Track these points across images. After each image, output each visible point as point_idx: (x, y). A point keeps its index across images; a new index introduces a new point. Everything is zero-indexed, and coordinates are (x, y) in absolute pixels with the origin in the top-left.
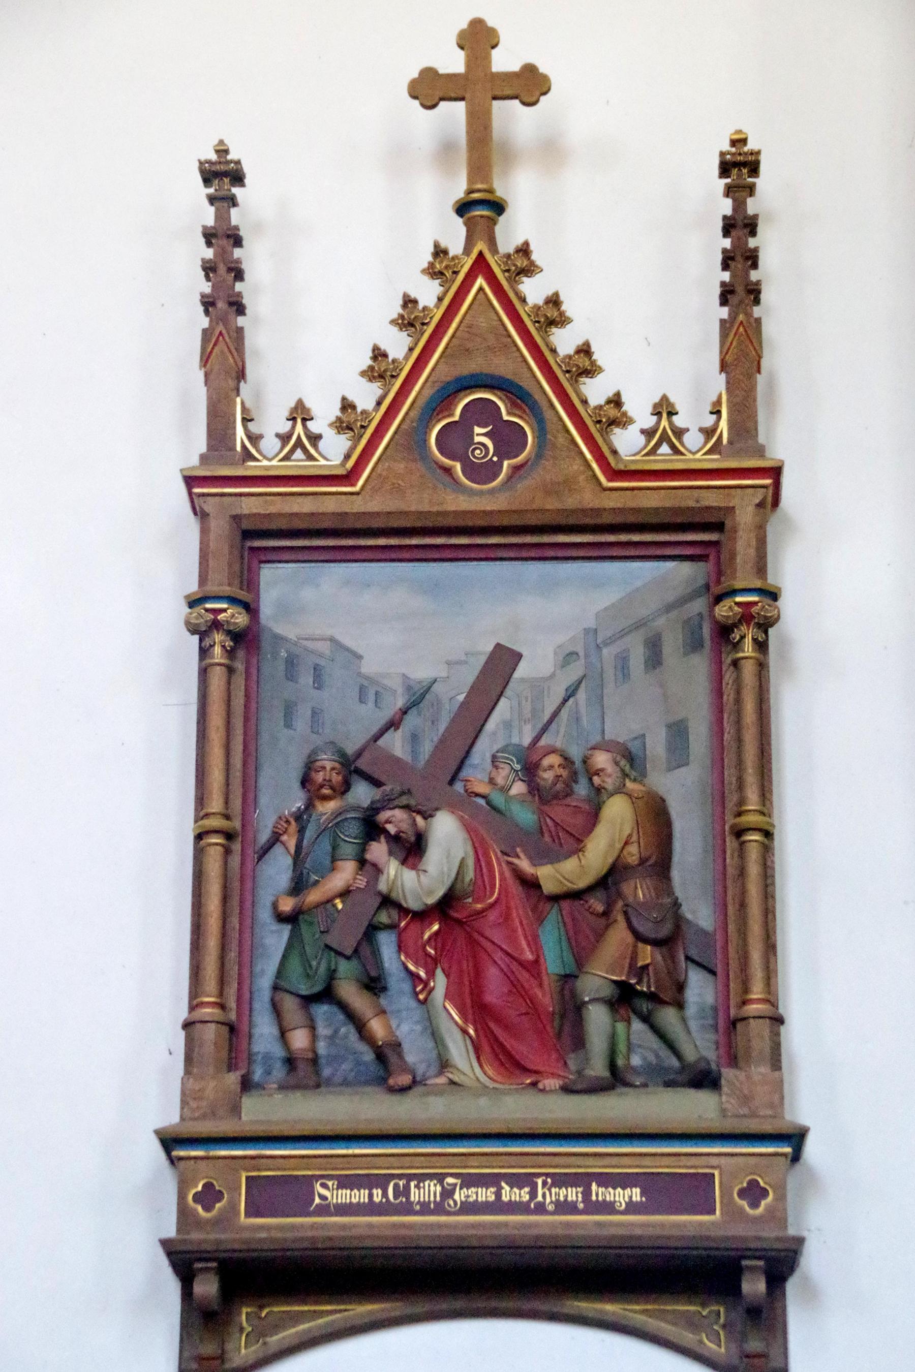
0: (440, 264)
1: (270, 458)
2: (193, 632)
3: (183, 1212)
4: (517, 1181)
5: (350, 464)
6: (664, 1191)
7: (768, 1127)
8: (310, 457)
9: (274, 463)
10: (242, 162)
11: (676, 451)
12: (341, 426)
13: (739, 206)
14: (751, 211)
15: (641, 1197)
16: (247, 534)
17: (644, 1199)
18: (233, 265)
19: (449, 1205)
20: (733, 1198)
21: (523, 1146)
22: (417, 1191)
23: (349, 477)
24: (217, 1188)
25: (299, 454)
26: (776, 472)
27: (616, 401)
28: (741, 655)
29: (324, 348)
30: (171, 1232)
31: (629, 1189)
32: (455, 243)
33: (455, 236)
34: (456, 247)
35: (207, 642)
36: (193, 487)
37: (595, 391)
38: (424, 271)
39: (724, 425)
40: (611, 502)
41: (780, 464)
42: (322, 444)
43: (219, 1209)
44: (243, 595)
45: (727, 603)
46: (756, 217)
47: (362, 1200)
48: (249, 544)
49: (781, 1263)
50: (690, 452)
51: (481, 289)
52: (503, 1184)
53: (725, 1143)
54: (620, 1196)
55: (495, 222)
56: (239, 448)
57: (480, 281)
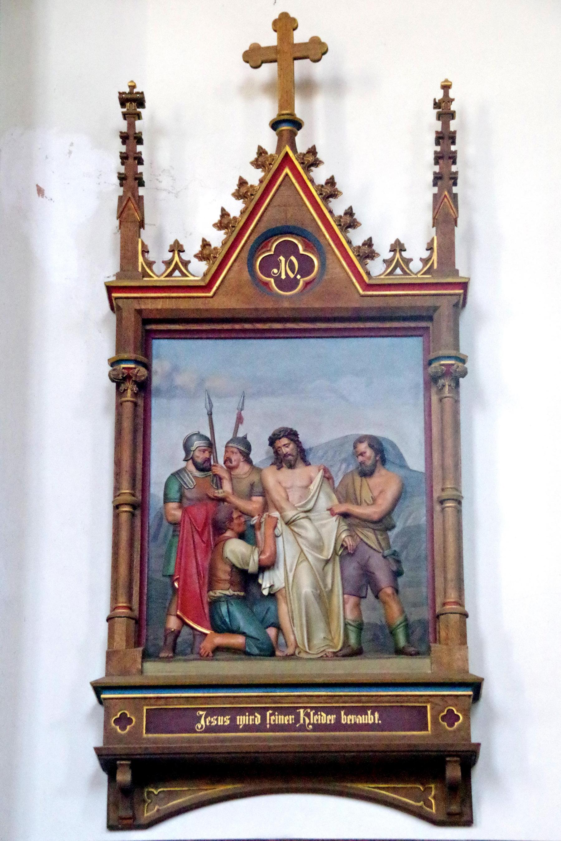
0: (261, 160)
1: (158, 275)
2: (113, 381)
3: (108, 734)
4: (284, 711)
5: (207, 280)
6: (392, 715)
7: (457, 678)
8: (184, 275)
9: (162, 278)
10: (145, 93)
11: (405, 273)
12: (201, 257)
13: (131, 126)
14: (452, 129)
15: (378, 720)
16: (146, 321)
17: (380, 722)
18: (137, 156)
19: (197, 727)
20: (438, 720)
21: (124, 694)
22: (372, 717)
23: (208, 287)
24: (128, 716)
25: (177, 273)
26: (464, 286)
27: (369, 243)
28: (124, 399)
29: (195, 208)
30: (100, 744)
31: (287, 717)
32: (271, 147)
33: (269, 141)
34: (271, 149)
35: (123, 387)
36: (112, 292)
37: (358, 237)
38: (252, 163)
39: (435, 257)
40: (366, 303)
41: (466, 281)
42: (190, 267)
43: (458, 725)
44: (141, 358)
45: (435, 364)
46: (455, 132)
47: (280, 722)
48: (149, 327)
49: (468, 758)
50: (157, 276)
51: (287, 175)
52: (256, 714)
53: (189, 690)
54: (370, 718)
55: (295, 134)
56: (140, 270)
57: (287, 170)
